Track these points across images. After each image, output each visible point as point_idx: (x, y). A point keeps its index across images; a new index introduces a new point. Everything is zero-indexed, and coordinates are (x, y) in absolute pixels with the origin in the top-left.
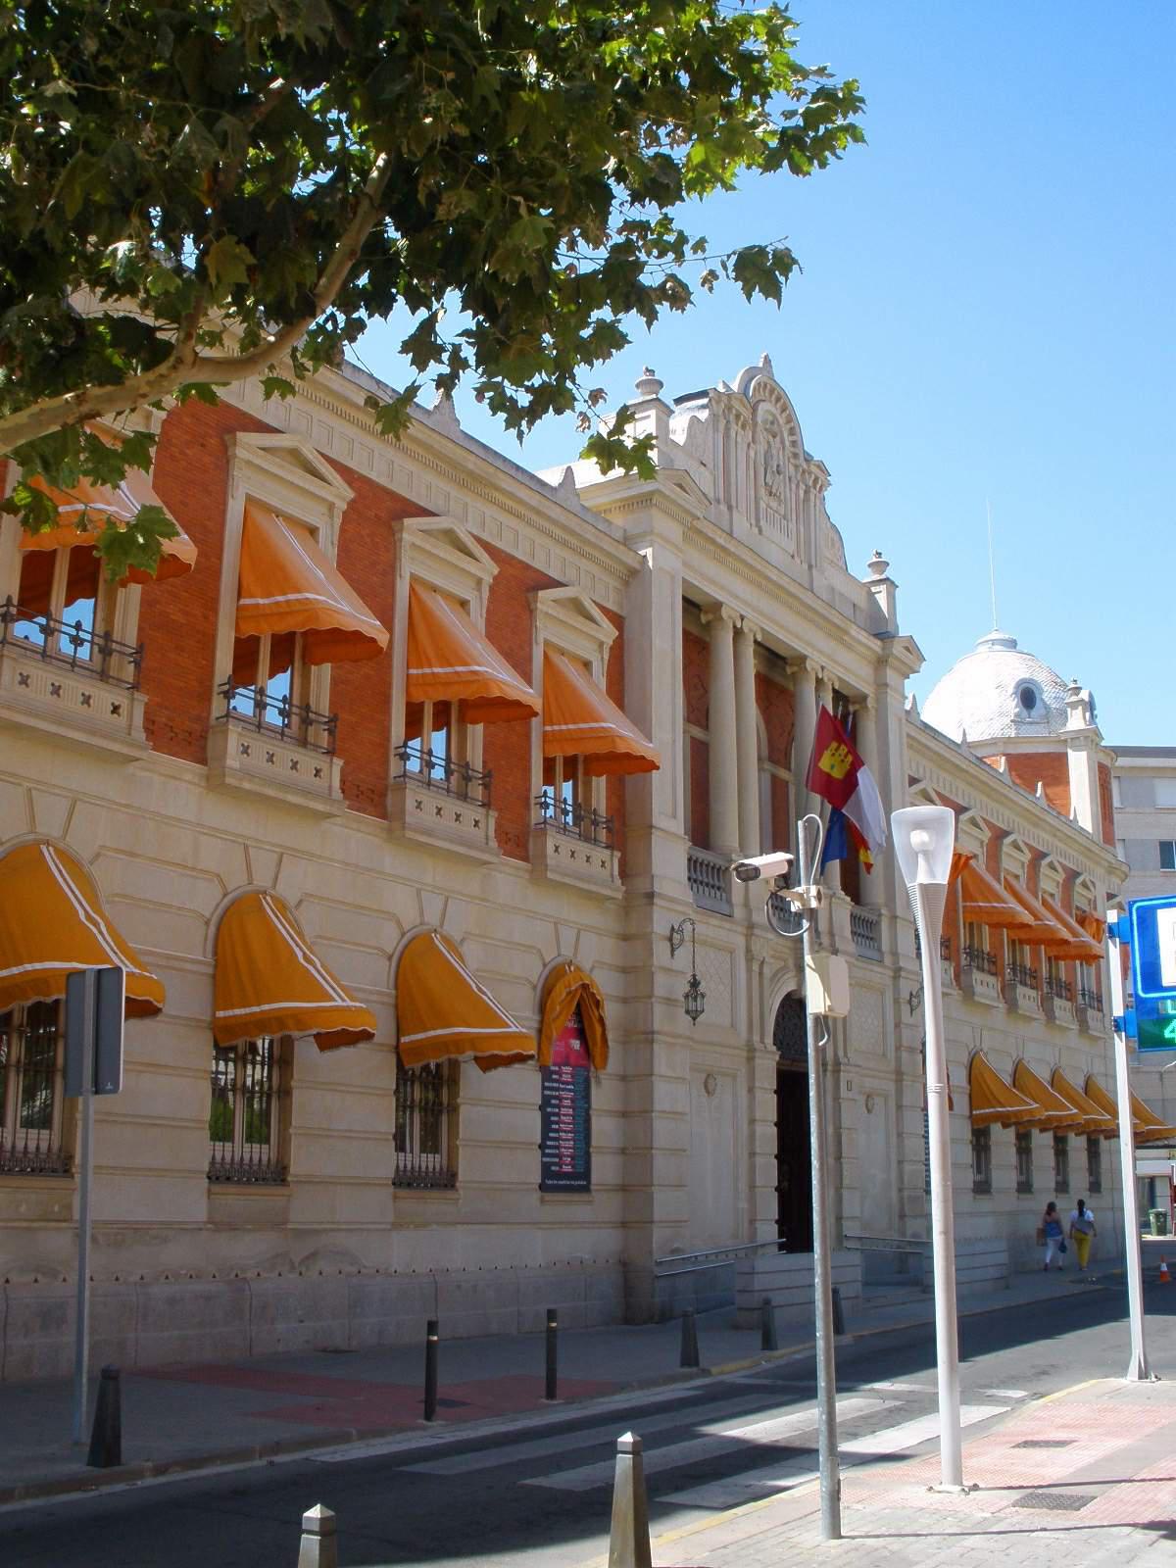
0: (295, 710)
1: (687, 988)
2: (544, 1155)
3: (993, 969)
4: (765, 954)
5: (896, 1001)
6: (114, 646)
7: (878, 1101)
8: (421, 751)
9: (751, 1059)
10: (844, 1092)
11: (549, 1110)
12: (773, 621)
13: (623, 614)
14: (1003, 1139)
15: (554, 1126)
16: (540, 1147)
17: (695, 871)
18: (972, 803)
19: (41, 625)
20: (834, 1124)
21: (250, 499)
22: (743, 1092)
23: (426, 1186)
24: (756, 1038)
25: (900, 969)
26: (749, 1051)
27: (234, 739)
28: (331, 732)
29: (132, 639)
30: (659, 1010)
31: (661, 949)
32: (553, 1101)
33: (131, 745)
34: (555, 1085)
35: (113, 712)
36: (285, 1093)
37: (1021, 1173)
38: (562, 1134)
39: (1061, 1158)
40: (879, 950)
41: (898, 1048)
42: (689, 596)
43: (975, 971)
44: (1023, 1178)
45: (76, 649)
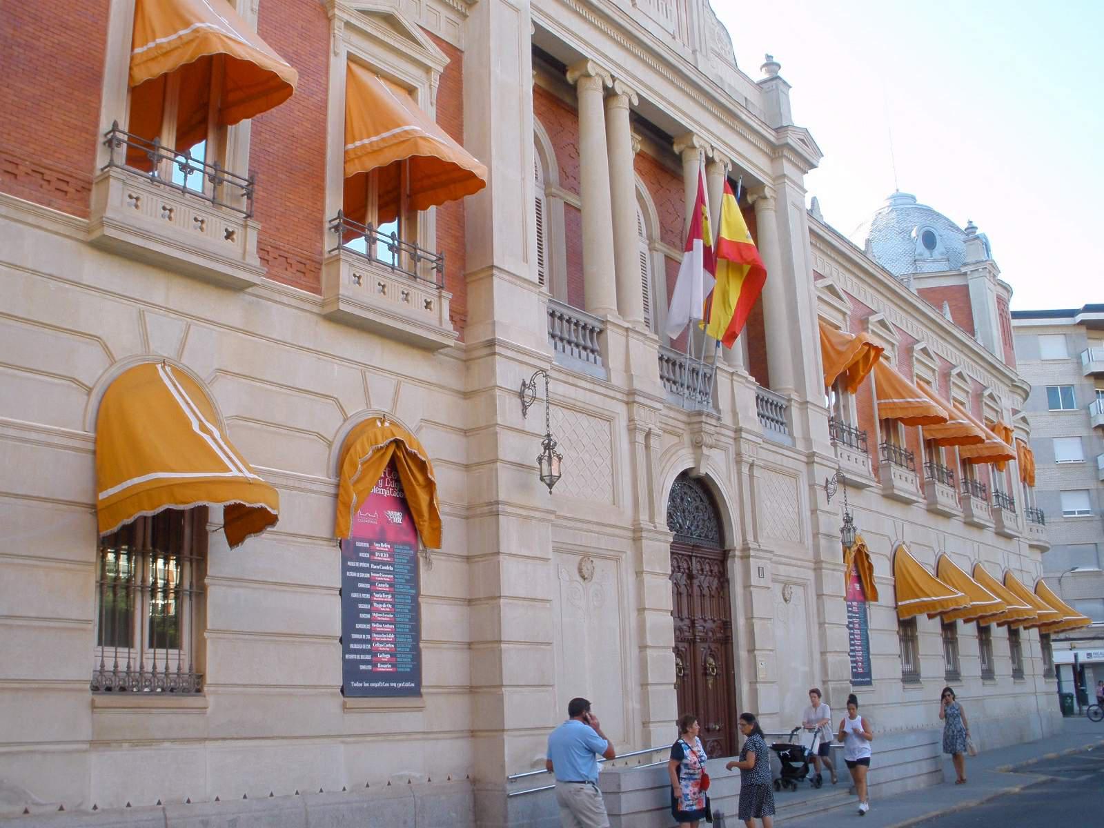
0: (403, 246)
1: (842, 524)
2: (346, 650)
3: (911, 465)
4: (650, 426)
5: (812, 486)
6: (226, 176)
7: (797, 591)
8: (205, 164)
9: (637, 540)
10: (754, 579)
11: (354, 595)
12: (650, 89)
13: (462, 48)
14: (929, 629)
15: (362, 616)
16: (341, 641)
17: (763, 409)
18: (881, 308)
19: (180, 163)
20: (746, 612)
21: (351, 58)
22: (630, 579)
23: (153, 691)
24: (644, 517)
25: (814, 454)
26: (816, 563)
27: (345, 272)
28: (249, 195)
29: (243, 171)
30: (505, 476)
31: (507, 410)
32: (361, 585)
33: (918, 497)
34: (363, 565)
35: (227, 238)
36: (200, 594)
37: (949, 662)
38: (378, 626)
39: (1046, 651)
40: (791, 434)
41: (816, 535)
42: (546, 49)
43: (893, 464)
44: (951, 668)
45: (186, 177)
